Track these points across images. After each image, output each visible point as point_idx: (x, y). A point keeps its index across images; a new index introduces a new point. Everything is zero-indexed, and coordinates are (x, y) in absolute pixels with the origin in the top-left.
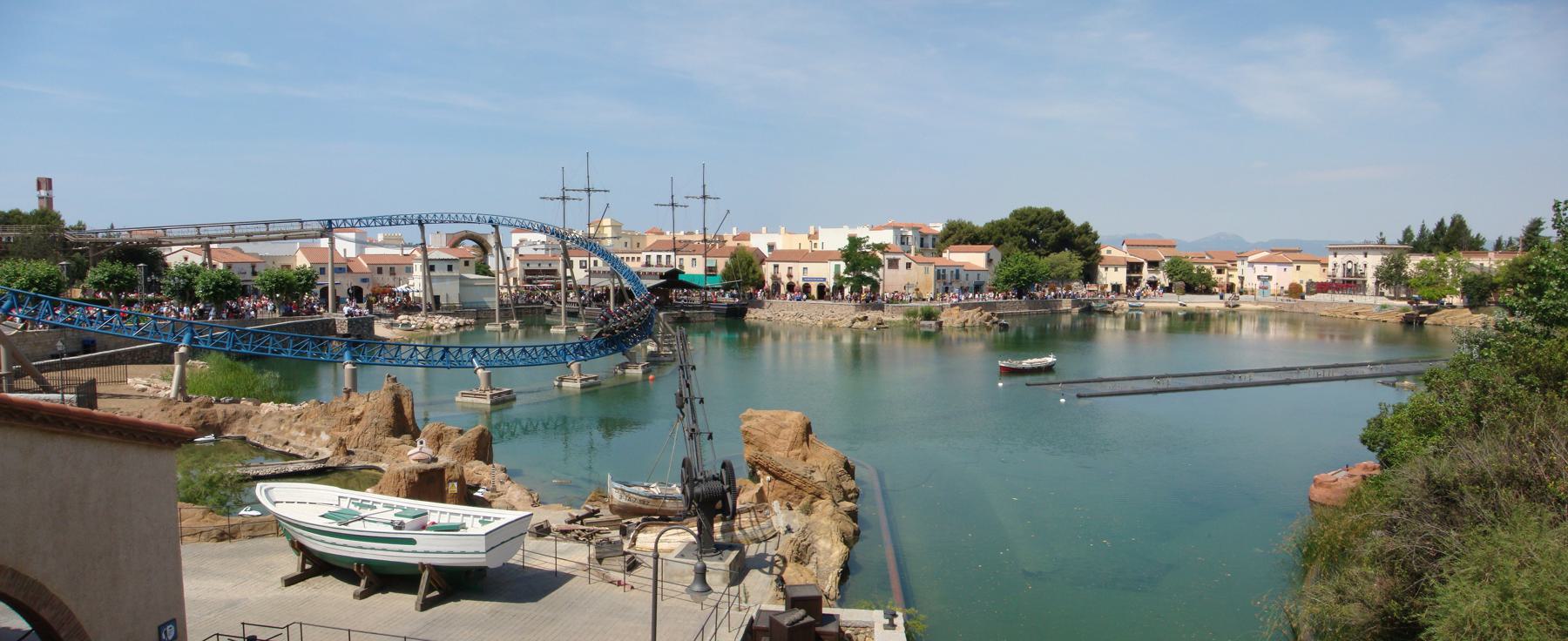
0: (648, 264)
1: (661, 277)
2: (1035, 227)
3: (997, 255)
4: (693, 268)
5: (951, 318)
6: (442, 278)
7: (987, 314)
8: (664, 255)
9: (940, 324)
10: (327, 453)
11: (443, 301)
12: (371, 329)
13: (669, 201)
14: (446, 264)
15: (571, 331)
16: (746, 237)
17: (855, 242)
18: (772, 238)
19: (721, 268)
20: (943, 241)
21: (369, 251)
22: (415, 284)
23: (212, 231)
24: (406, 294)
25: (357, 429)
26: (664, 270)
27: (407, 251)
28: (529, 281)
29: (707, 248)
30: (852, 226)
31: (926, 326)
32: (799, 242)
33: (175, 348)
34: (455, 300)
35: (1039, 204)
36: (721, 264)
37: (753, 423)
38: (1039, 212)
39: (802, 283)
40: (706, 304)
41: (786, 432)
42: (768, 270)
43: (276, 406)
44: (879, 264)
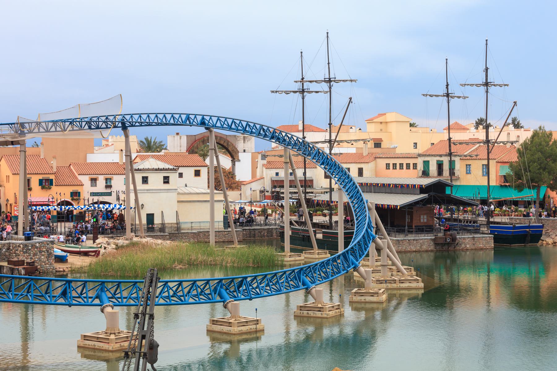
1: (422, 190)
11: (157, 221)
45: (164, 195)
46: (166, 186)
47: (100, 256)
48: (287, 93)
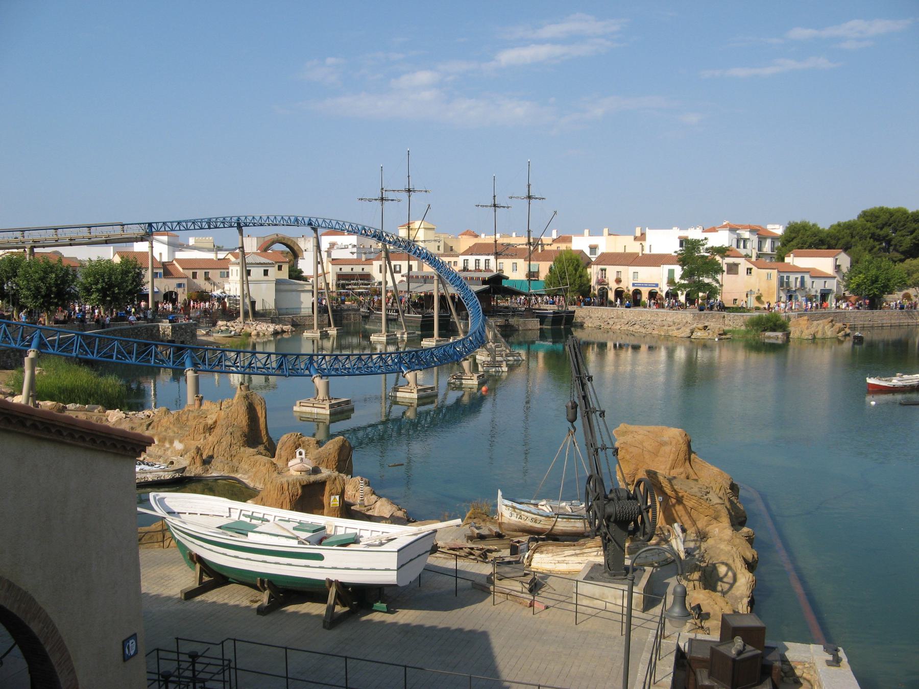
0: (465, 269)
1: (484, 282)
2: (888, 230)
3: (845, 260)
4: (515, 271)
5: (800, 329)
6: (257, 282)
7: (840, 325)
8: (482, 258)
9: (788, 335)
10: (184, 462)
11: (258, 307)
12: (194, 335)
13: (491, 202)
14: (262, 270)
15: (391, 341)
16: (568, 240)
17: (690, 246)
18: (594, 241)
19: (544, 273)
20: (784, 245)
21: (180, 255)
22: (233, 286)
23: (36, 235)
24: (220, 299)
25: (211, 439)
26: (487, 275)
27: (221, 255)
28: (343, 286)
29: (533, 250)
30: (682, 228)
31: (766, 334)
32: (625, 244)
33: (23, 354)
34: (271, 305)
35: (892, 204)
36: (544, 269)
37: (629, 438)
38: (891, 213)
39: (632, 289)
40: (530, 312)
41: (667, 449)
42: (593, 272)
43: (121, 414)
44: (718, 270)
45: (264, 286)
46: (266, 278)
47: (864, 345)
48: (370, 200)
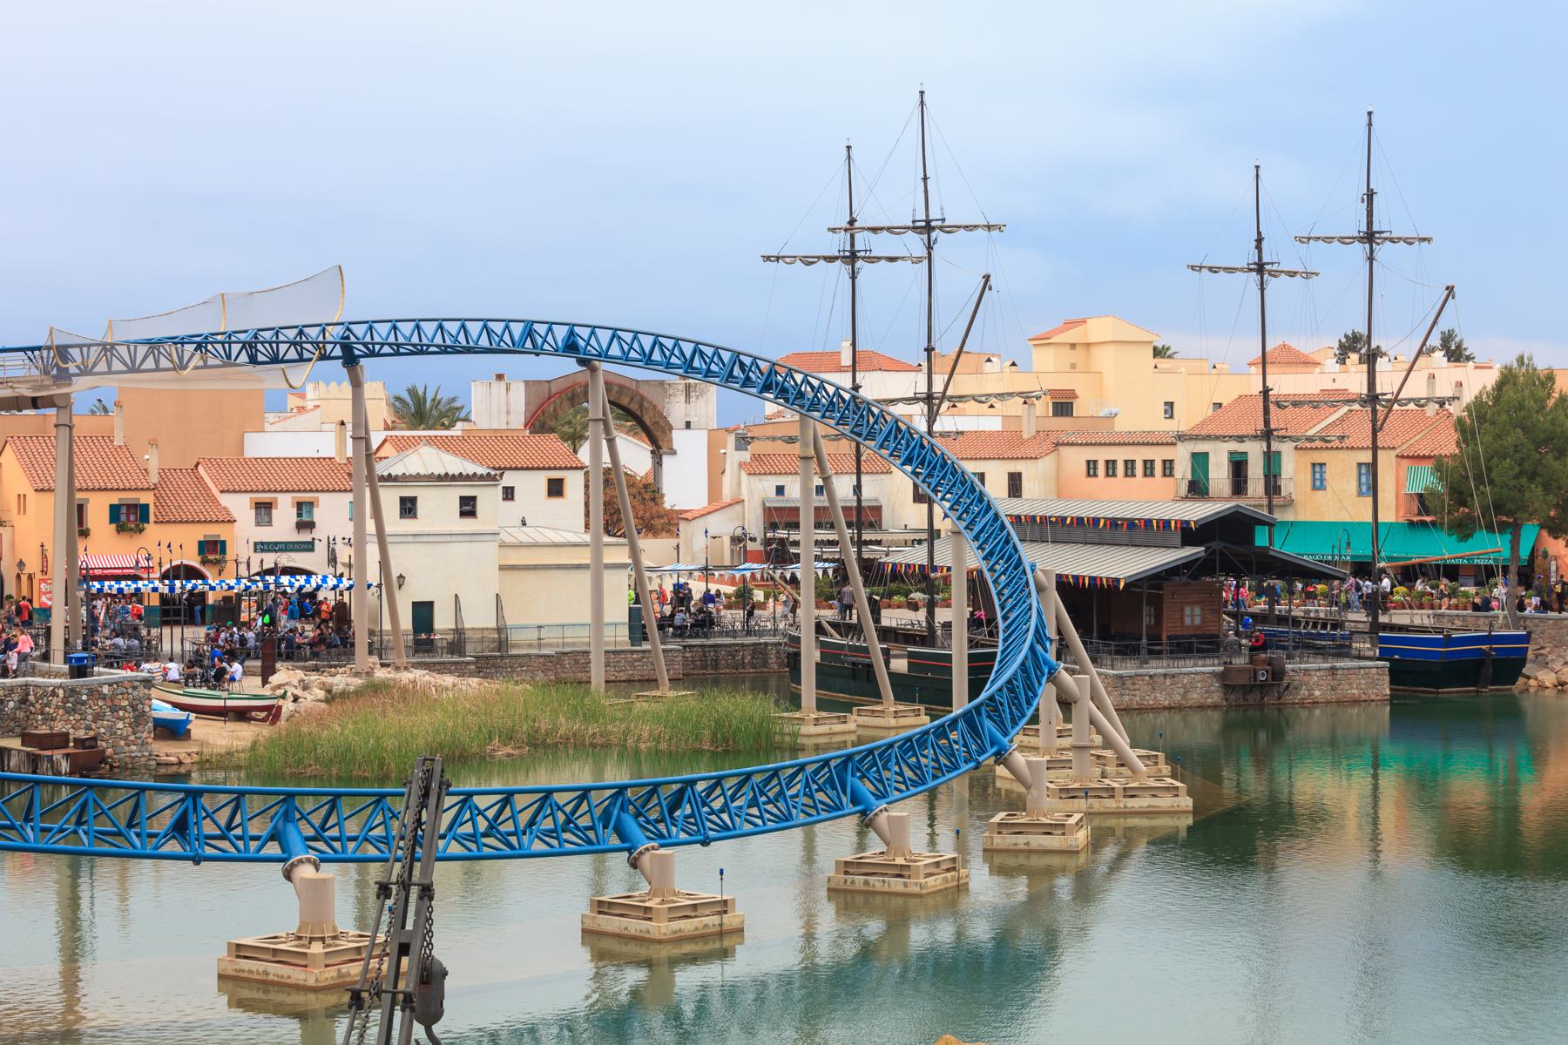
1: (1189, 534)
11: (443, 621)
45: (460, 550)
46: (468, 525)
47: (282, 722)
48: (808, 261)
